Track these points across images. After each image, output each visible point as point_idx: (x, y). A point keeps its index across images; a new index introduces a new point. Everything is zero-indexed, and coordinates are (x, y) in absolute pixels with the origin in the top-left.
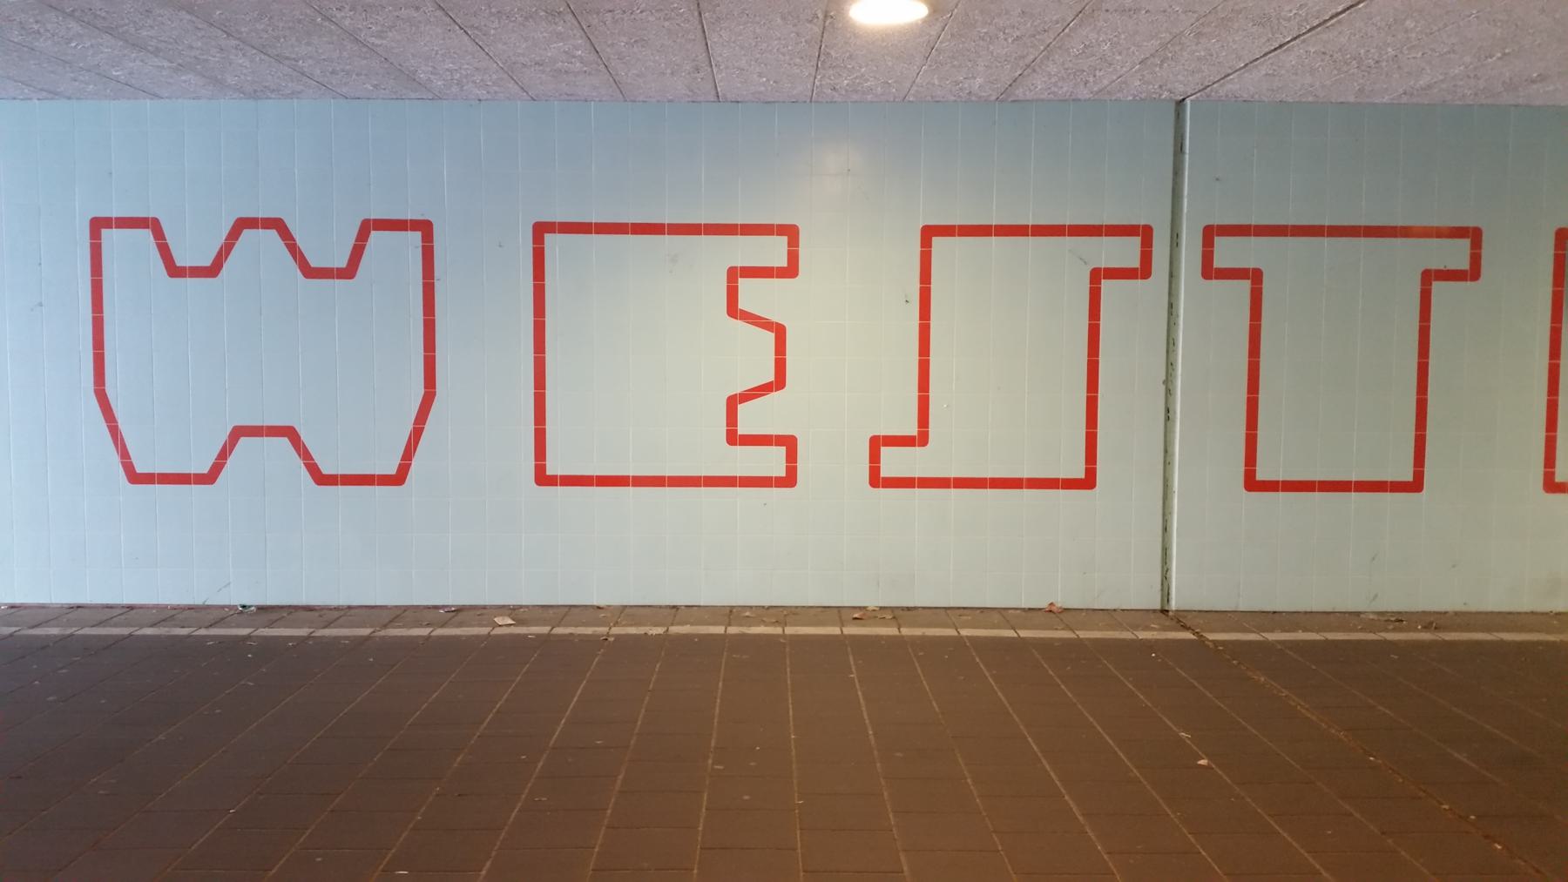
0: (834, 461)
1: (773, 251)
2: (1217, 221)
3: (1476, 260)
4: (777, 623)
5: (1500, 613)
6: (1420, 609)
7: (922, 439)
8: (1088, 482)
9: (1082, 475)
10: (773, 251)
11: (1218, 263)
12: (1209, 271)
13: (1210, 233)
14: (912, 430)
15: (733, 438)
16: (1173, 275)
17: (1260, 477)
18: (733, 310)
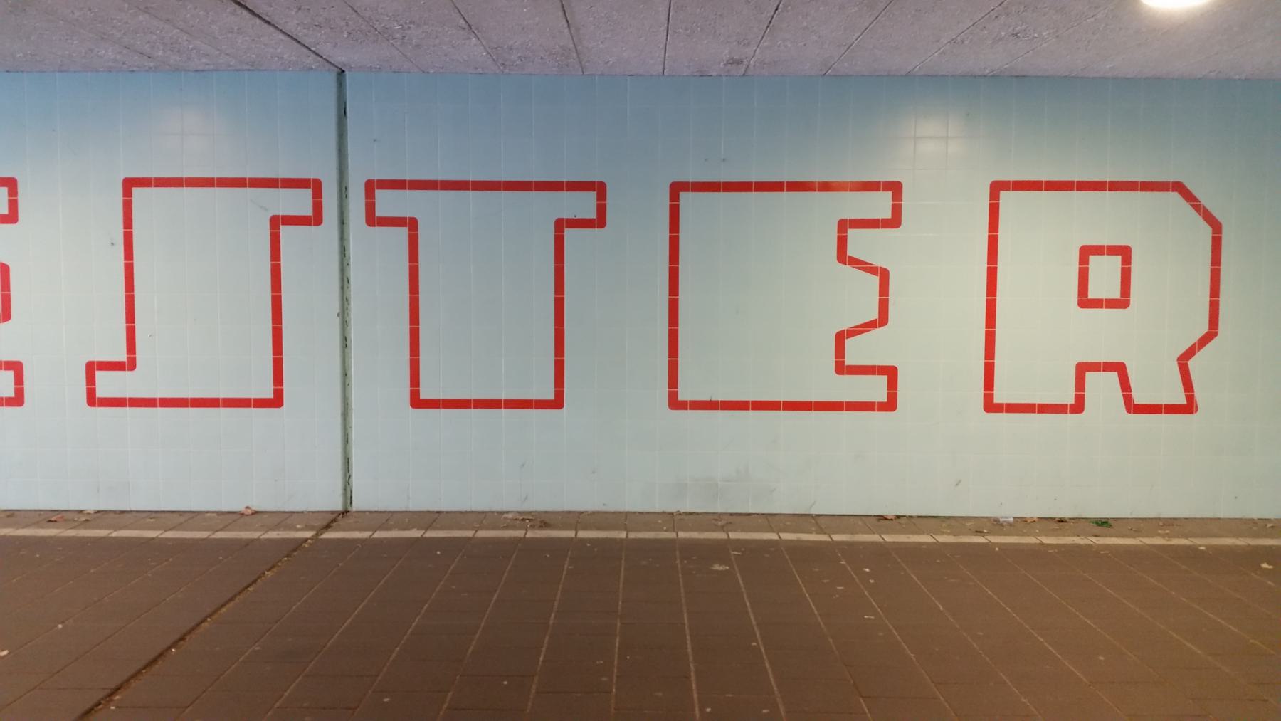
0: (52, 383)
1: (880, 205)
2: (376, 177)
3: (602, 210)
4: (722, 529)
5: (1203, 519)
6: (566, 509)
7: (131, 364)
8: (276, 401)
9: (552, 397)
10: (880, 205)
11: (380, 212)
12: (372, 219)
13: (371, 187)
14: (122, 357)
15: (841, 368)
16: (342, 222)
17: (423, 396)
18: (843, 256)
